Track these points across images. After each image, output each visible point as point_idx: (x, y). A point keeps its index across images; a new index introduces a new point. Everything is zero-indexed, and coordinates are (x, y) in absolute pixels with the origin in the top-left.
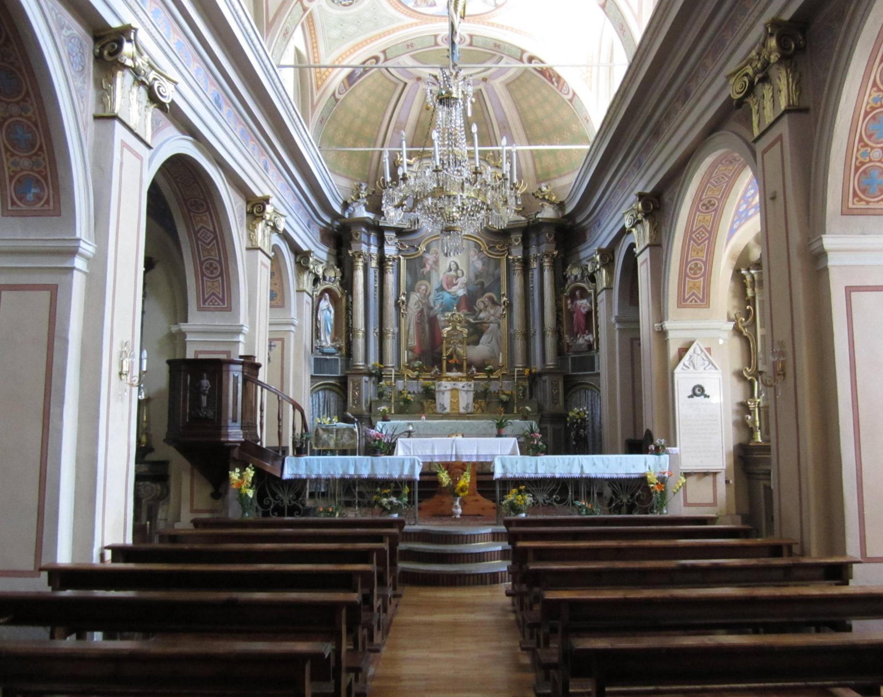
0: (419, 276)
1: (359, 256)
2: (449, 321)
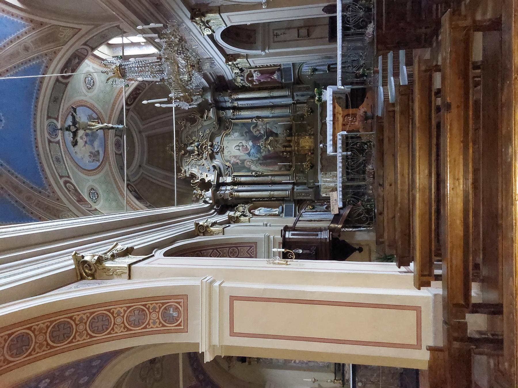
0: (242, 166)
1: (232, 194)
2: (265, 147)
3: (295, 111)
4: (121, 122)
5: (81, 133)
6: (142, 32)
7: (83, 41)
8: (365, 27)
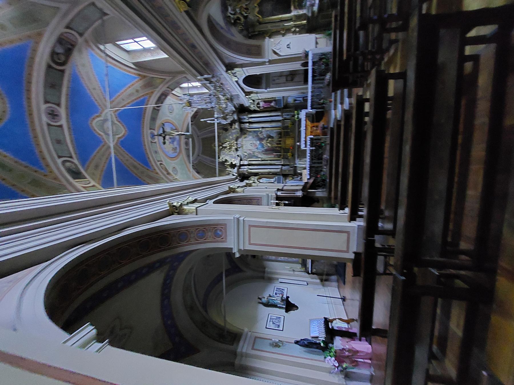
3: (283, 124)
4: (188, 131)
5: (167, 137)
6: (199, 81)
7: (167, 85)
8: (325, 75)
